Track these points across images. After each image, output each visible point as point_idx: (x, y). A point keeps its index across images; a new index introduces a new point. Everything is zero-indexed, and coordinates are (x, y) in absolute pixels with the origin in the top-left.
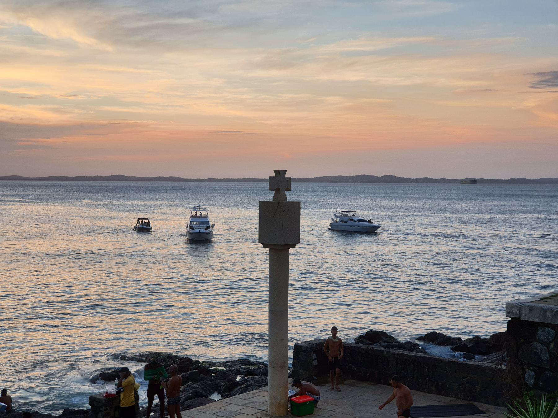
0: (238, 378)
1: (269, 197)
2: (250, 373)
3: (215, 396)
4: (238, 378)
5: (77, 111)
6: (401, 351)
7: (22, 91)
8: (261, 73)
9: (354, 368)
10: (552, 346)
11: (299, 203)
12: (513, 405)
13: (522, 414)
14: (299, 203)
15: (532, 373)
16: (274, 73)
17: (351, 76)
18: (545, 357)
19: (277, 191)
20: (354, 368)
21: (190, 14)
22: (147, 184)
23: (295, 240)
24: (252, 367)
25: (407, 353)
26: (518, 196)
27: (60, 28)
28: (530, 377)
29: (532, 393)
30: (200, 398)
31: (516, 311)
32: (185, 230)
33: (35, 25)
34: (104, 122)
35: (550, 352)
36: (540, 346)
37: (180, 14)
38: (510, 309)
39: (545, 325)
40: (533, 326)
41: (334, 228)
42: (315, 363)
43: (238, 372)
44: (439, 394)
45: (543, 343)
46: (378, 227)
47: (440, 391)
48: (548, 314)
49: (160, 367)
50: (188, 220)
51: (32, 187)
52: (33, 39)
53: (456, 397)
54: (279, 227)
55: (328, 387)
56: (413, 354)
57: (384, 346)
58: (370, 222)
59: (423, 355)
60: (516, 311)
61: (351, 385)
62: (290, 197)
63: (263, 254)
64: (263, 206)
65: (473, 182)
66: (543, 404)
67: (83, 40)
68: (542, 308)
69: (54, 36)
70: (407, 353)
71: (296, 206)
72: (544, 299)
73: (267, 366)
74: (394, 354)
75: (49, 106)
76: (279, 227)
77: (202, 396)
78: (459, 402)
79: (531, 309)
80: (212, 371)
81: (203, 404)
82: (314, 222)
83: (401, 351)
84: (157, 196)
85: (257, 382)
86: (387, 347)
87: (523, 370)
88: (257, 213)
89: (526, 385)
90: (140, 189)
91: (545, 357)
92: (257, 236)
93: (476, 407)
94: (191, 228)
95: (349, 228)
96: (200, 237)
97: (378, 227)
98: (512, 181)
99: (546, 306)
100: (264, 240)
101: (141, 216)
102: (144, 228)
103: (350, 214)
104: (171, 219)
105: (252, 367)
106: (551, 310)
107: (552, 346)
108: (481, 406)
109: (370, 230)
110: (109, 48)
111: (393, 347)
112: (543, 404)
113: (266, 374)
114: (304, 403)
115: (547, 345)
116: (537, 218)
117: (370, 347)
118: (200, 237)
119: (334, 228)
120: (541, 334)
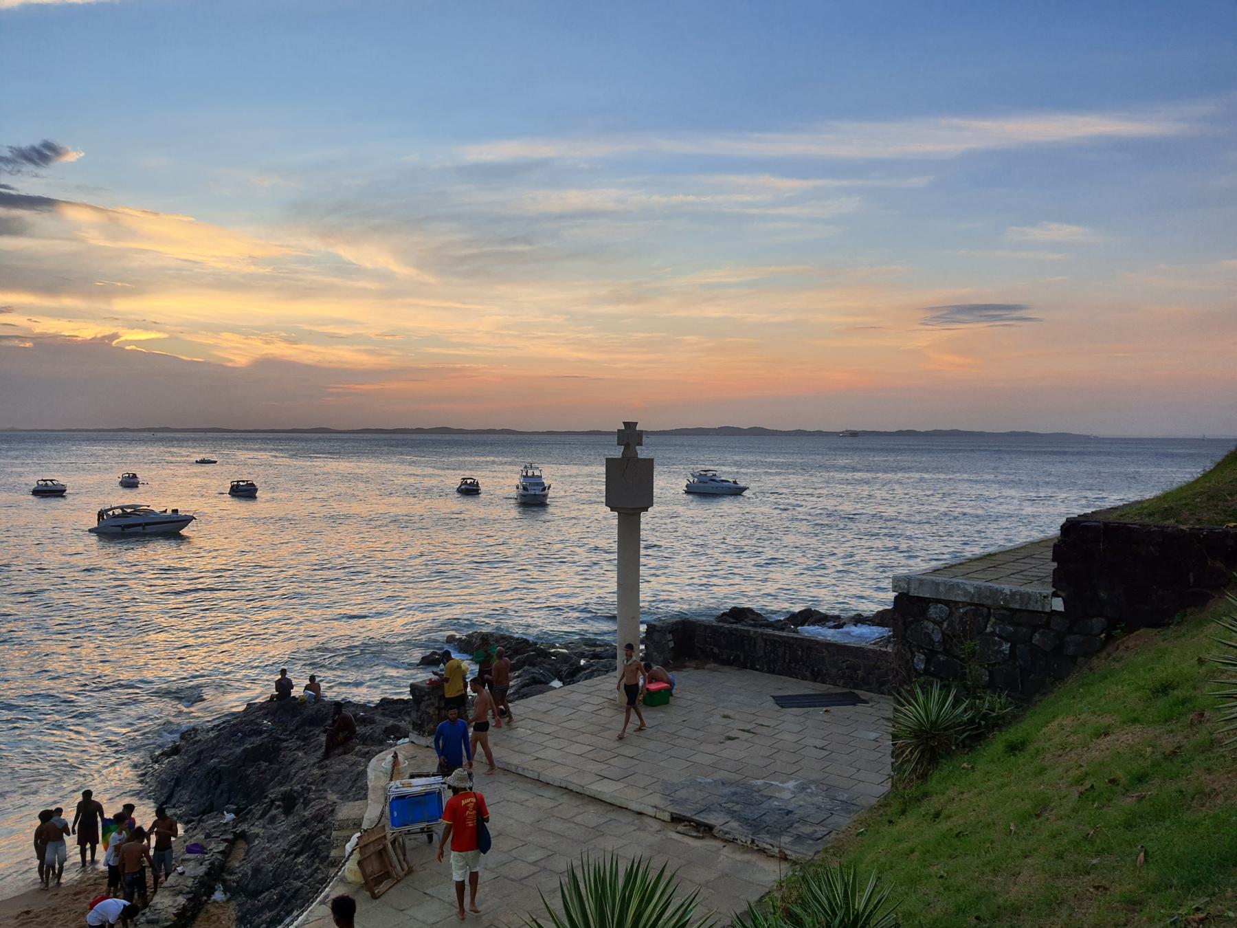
0: (582, 662)
1: (617, 452)
2: (596, 656)
3: (556, 683)
4: (582, 662)
5: (395, 353)
6: (770, 631)
7: (330, 329)
8: (607, 309)
9: (716, 650)
10: (945, 625)
11: (652, 460)
12: (899, 694)
13: (910, 704)
14: (652, 460)
15: (922, 657)
16: (624, 308)
17: (713, 312)
18: (937, 637)
19: (627, 446)
20: (716, 650)
21: (527, 240)
22: (476, 437)
23: (647, 502)
24: (598, 649)
25: (777, 633)
26: (861, 450)
27: (374, 255)
28: (920, 662)
29: (922, 679)
30: (536, 685)
31: (904, 585)
32: (514, 493)
33: (346, 253)
34: (426, 366)
35: (943, 633)
36: (931, 625)
37: (514, 240)
38: (897, 581)
39: (939, 601)
40: (924, 603)
41: (689, 491)
42: (671, 644)
43: (582, 656)
44: (815, 681)
45: (935, 622)
46: (745, 489)
47: (816, 677)
48: (941, 589)
49: (481, 645)
50: (517, 480)
51: (306, 440)
52: (345, 269)
53: (835, 684)
54: (629, 489)
55: (684, 673)
56: (784, 634)
57: (750, 625)
58: (735, 482)
59: (796, 636)
60: (904, 585)
61: (712, 670)
62: (643, 453)
63: (613, 518)
64: (610, 464)
65: (854, 434)
66: (936, 693)
67: (401, 270)
68: (933, 582)
69: (368, 265)
70: (777, 633)
71: (649, 465)
72: (936, 571)
73: (615, 648)
74: (762, 634)
75: (362, 347)
76: (629, 489)
77: (540, 682)
78: (839, 690)
79: (921, 582)
80: (553, 654)
81: (541, 692)
82: (668, 484)
83: (770, 631)
84: (461, 451)
85: (604, 666)
86: (754, 626)
87: (912, 653)
88: (603, 469)
89: (916, 670)
90: (473, 444)
91: (937, 637)
92: (604, 500)
93: (857, 696)
94: (525, 489)
95: (706, 489)
96: (533, 499)
97: (745, 489)
98: (900, 433)
99: (939, 579)
100: (611, 503)
101: (467, 474)
102: (469, 490)
103: (710, 474)
104: (501, 479)
105: (598, 649)
106: (945, 583)
107: (945, 625)
108: (861, 693)
109: (736, 491)
110: (430, 279)
111: (761, 626)
112: (936, 693)
113: (614, 657)
114: (659, 691)
115: (940, 624)
116: (922, 480)
117: (734, 626)
118: (533, 499)
119: (689, 491)
120: (933, 611)
